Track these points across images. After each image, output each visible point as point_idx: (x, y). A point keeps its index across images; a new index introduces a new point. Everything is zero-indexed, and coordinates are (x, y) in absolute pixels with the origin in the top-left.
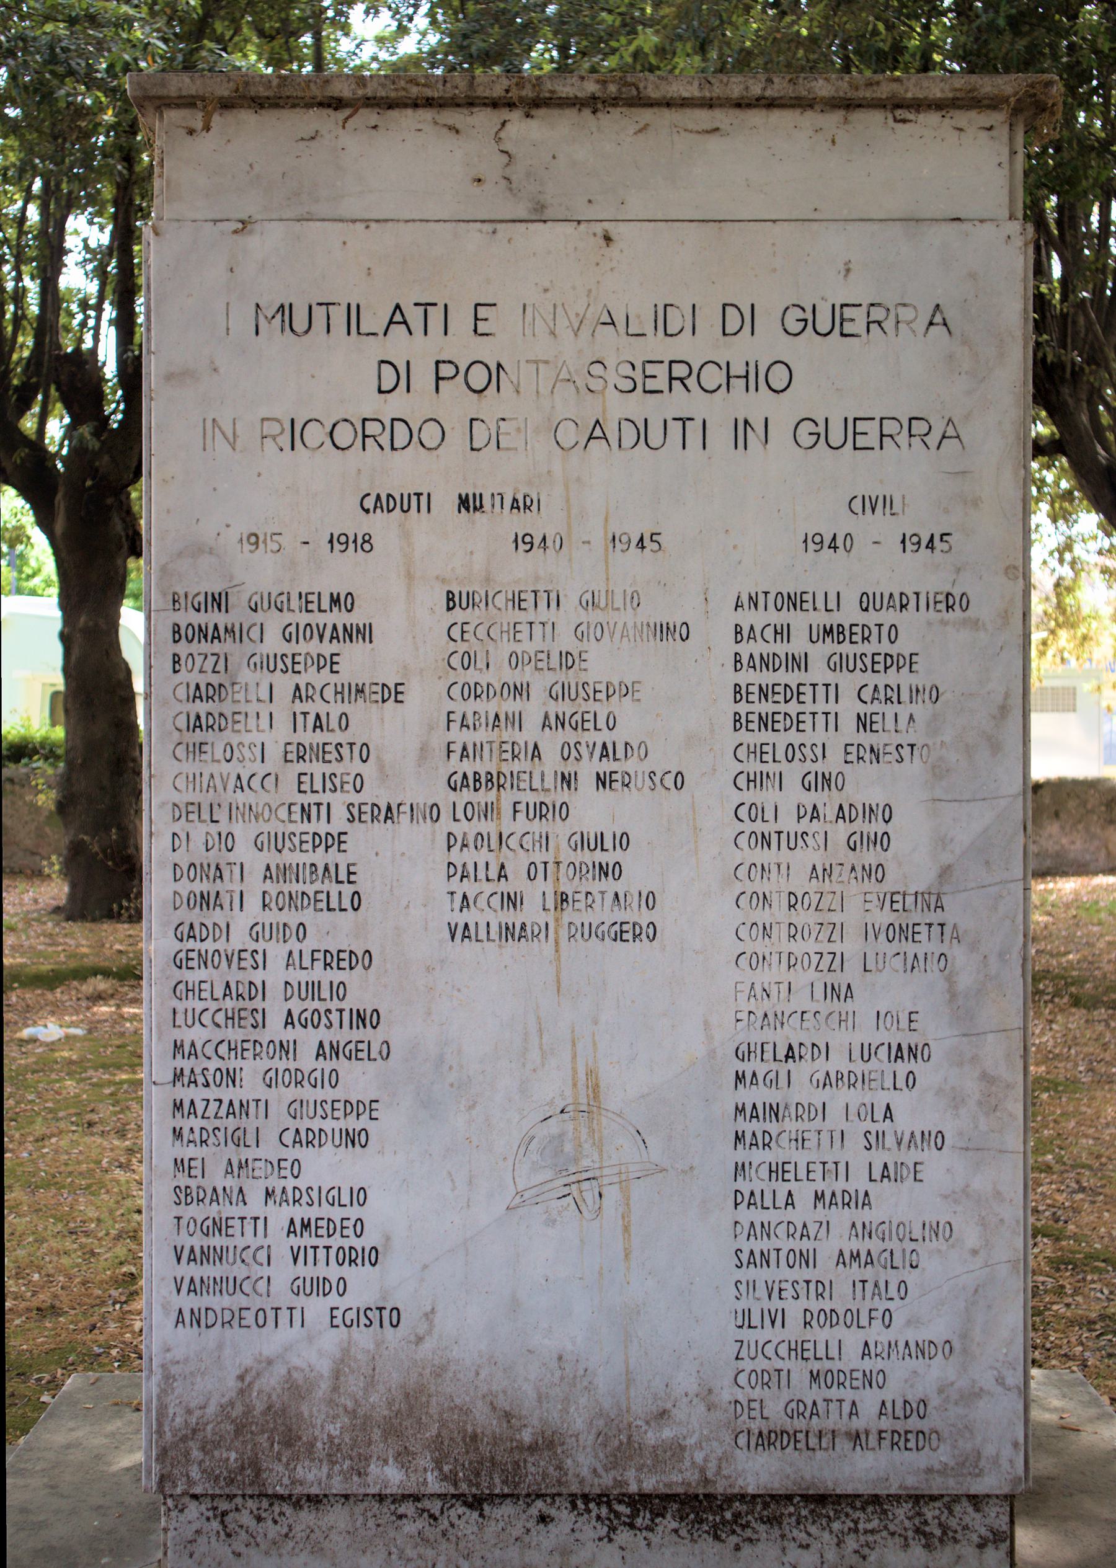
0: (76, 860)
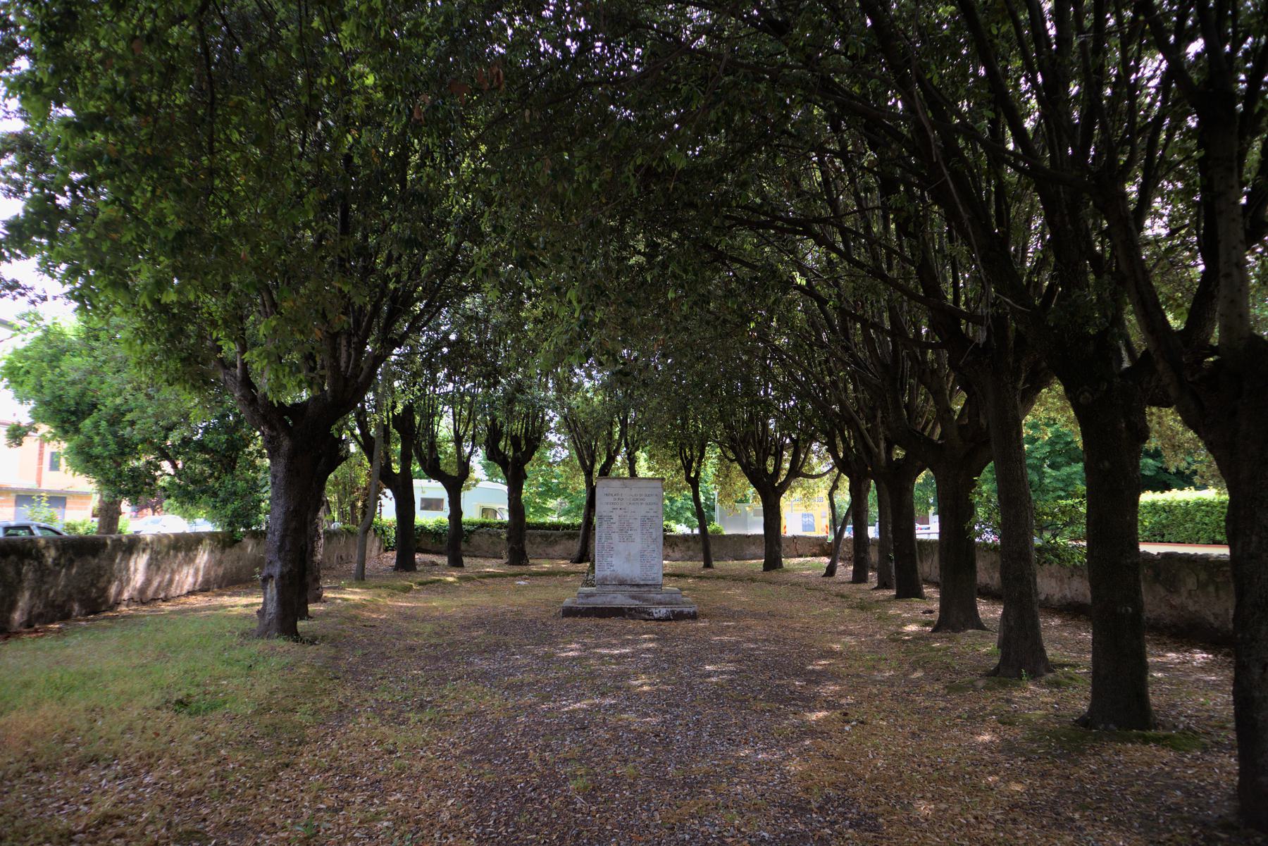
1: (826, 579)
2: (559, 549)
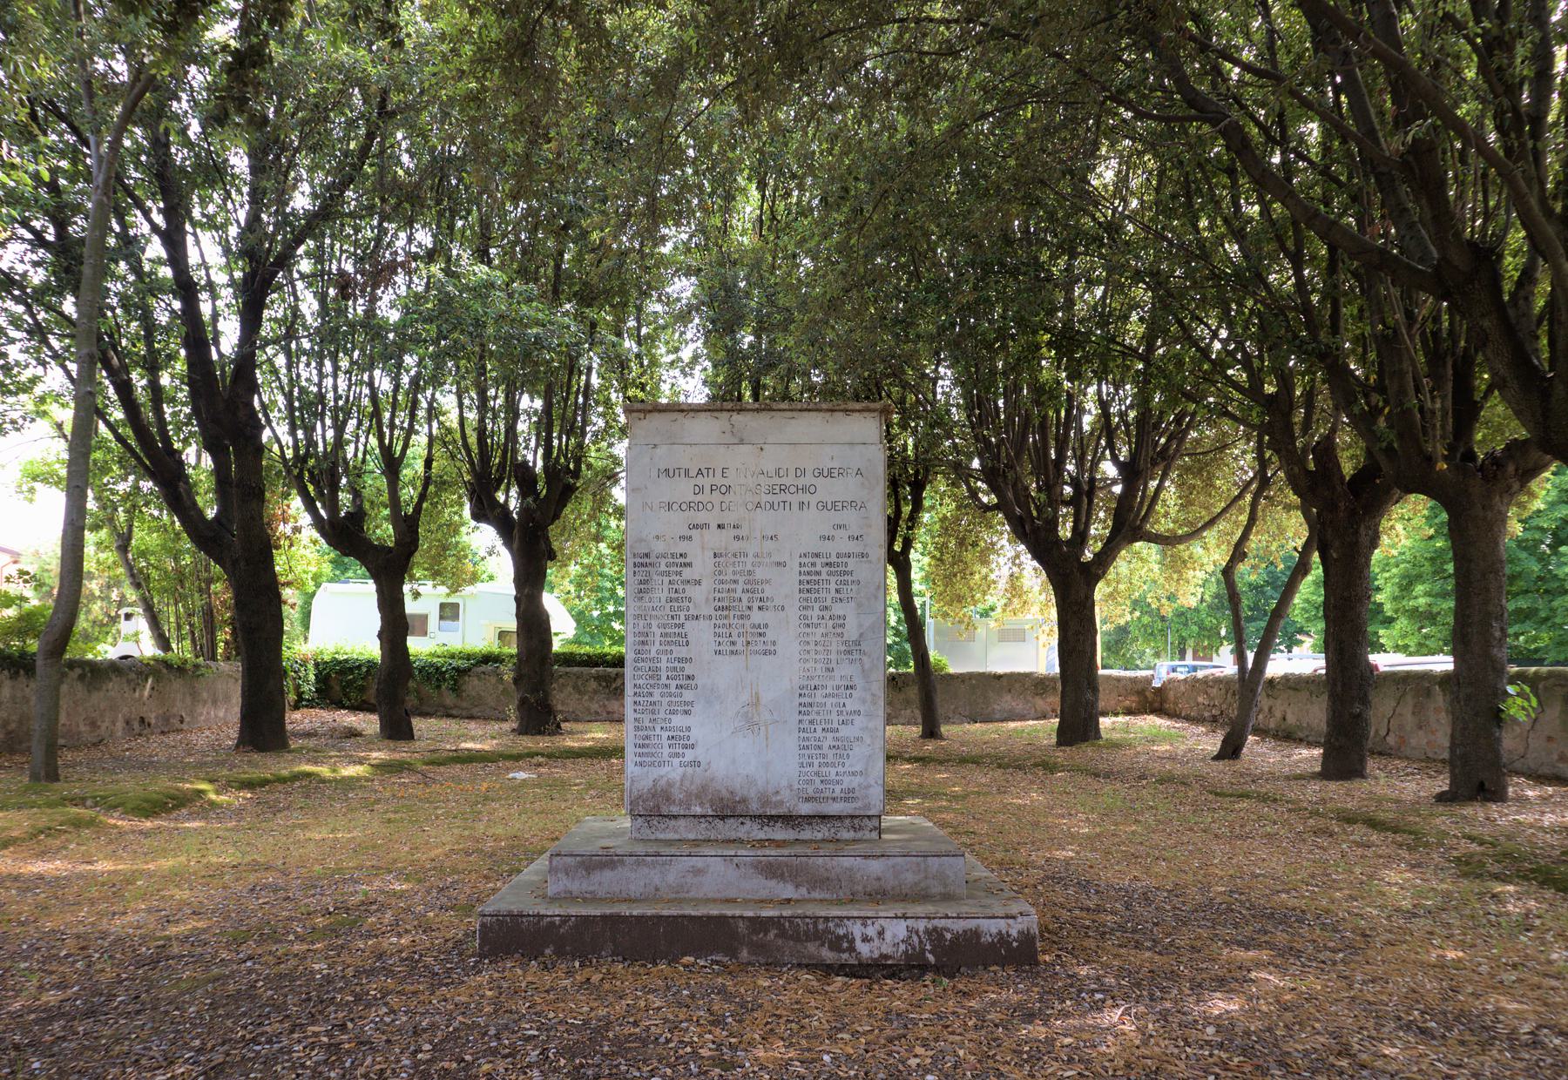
1: (1220, 764)
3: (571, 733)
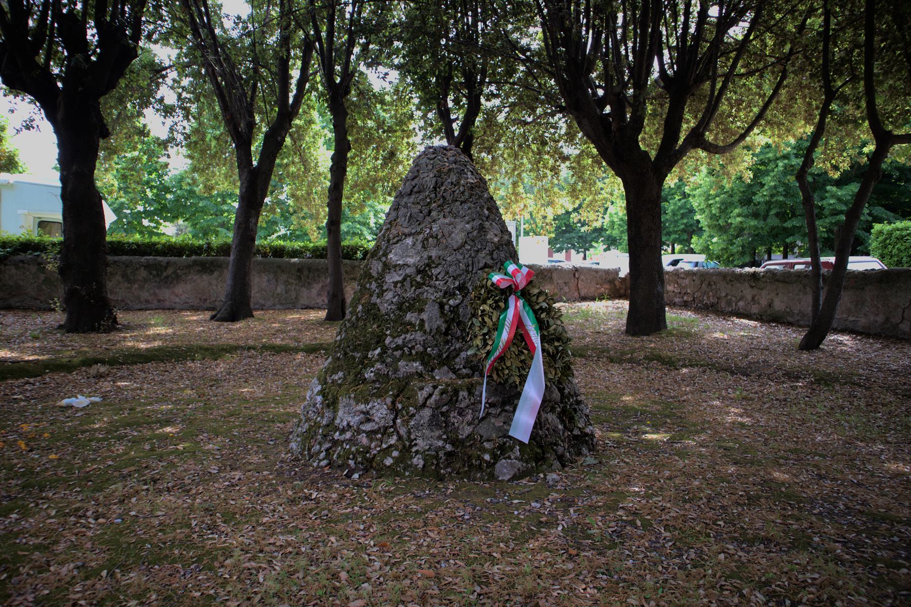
0: (72, 302)
2: (183, 291)
3: (128, 328)
